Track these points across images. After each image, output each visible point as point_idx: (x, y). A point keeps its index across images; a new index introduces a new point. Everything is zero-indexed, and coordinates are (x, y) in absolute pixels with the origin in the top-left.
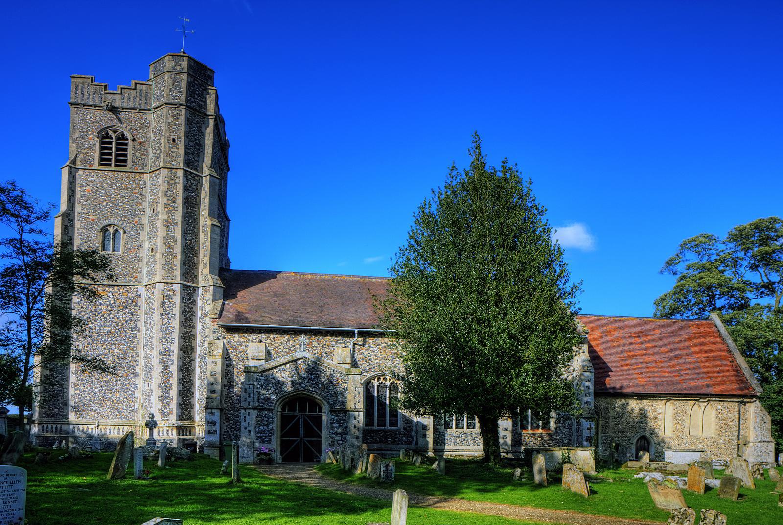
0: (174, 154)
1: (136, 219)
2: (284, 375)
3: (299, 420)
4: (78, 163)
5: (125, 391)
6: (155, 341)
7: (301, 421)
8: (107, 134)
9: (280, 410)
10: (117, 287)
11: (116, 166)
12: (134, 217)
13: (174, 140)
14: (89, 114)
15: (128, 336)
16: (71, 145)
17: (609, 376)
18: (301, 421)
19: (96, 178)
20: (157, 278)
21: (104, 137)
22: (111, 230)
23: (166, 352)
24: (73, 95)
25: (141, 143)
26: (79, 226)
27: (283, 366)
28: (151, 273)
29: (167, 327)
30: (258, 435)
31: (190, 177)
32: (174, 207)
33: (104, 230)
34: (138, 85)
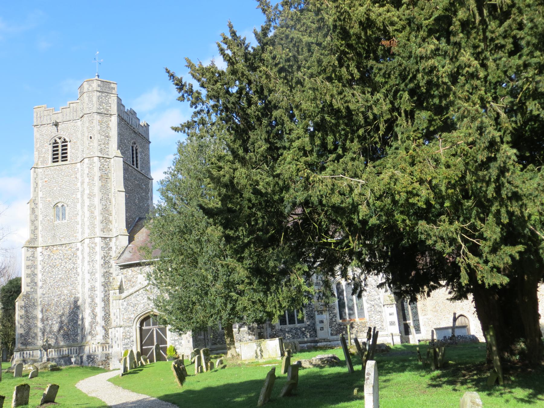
0: (91, 147)
1: (74, 196)
2: (138, 299)
3: (153, 330)
4: (40, 164)
6: (86, 282)
7: (155, 332)
8: (56, 141)
10: (64, 246)
11: (62, 161)
12: (73, 194)
13: (91, 138)
14: (44, 129)
15: (72, 279)
16: (35, 153)
18: (155, 332)
20: (86, 235)
22: (60, 205)
24: (35, 120)
26: (41, 207)
27: (137, 293)
28: (83, 233)
29: (93, 270)
30: (124, 346)
31: (103, 160)
32: (93, 184)
33: (56, 206)
34: (71, 105)
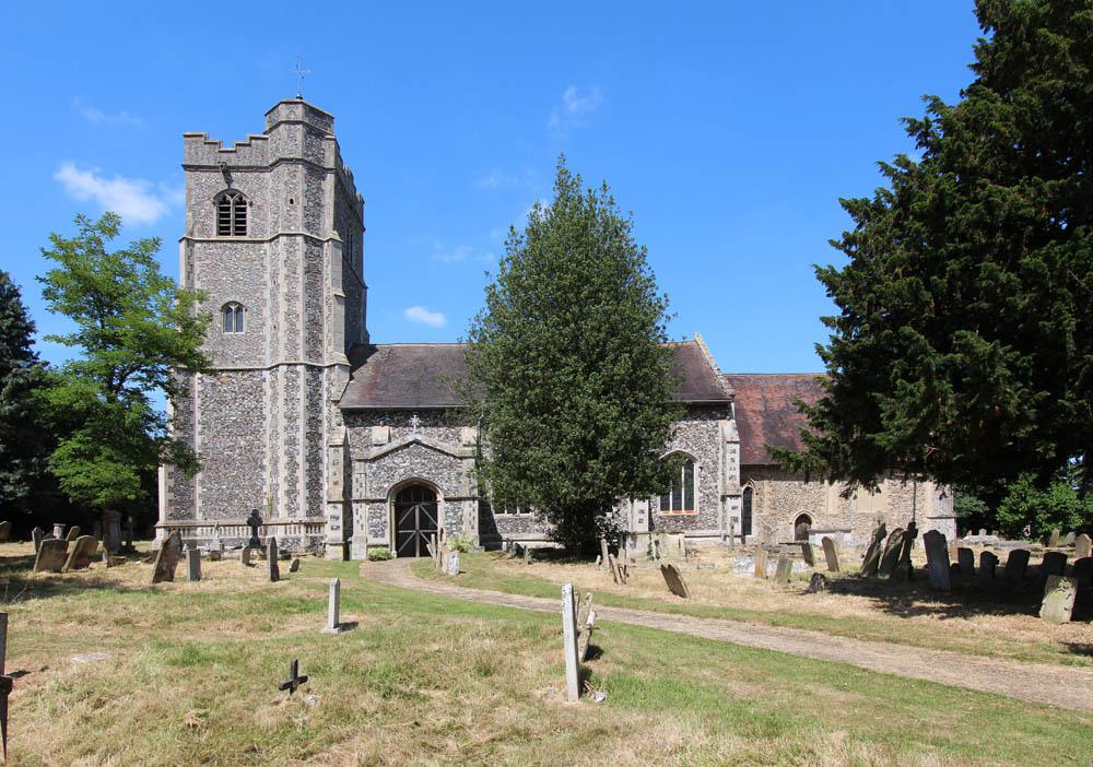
8: (225, 198)
12: (256, 291)
13: (292, 201)
23: (292, 442)
25: (259, 207)
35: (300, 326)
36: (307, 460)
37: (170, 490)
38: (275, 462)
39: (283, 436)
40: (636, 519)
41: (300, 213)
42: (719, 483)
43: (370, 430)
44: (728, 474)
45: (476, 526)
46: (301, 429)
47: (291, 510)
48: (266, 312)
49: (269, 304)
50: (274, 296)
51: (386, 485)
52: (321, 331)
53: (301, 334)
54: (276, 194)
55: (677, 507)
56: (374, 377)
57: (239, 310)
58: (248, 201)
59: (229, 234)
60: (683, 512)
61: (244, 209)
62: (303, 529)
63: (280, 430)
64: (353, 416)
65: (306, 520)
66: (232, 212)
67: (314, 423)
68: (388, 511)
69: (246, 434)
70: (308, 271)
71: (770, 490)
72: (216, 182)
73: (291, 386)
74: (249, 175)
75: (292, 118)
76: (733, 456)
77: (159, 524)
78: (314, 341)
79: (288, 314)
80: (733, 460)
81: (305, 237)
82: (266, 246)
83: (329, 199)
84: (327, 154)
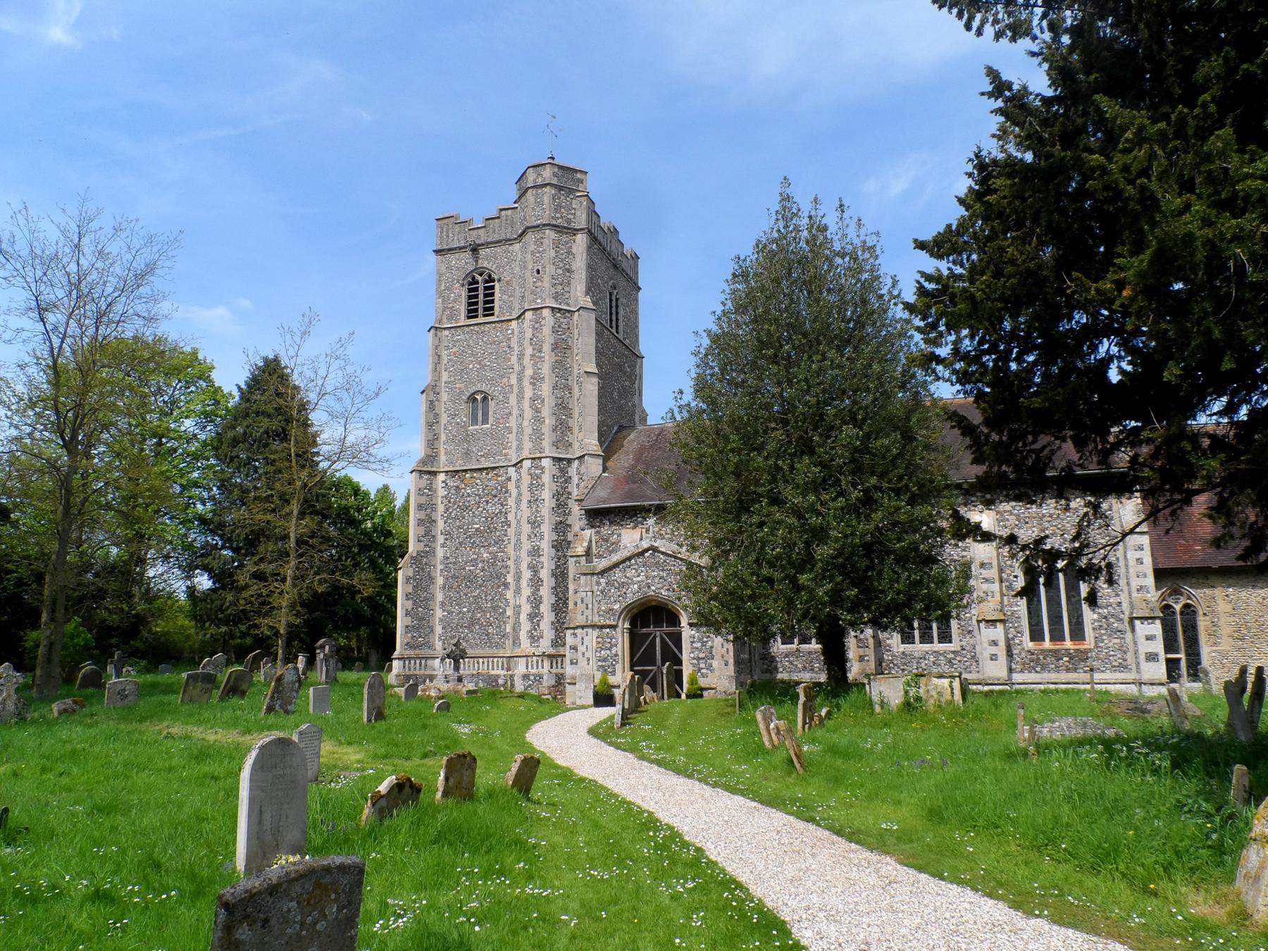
3: (655, 637)
5: (495, 608)
7: (658, 640)
8: (474, 278)
9: (627, 625)
12: (502, 377)
13: (538, 272)
17: (977, 477)
18: (658, 640)
19: (462, 337)
21: (470, 284)
23: (535, 552)
25: (508, 282)
33: (472, 398)
35: (546, 412)
36: (554, 575)
37: (407, 613)
38: (518, 577)
39: (526, 546)
40: (986, 654)
41: (547, 283)
42: (1124, 598)
43: (619, 535)
44: (1135, 583)
45: (731, 661)
46: (546, 537)
47: (534, 639)
48: (513, 399)
49: (516, 390)
50: (520, 380)
51: (617, 607)
52: (570, 416)
53: (547, 421)
54: (524, 267)
55: (1057, 636)
56: (634, 467)
57: (485, 399)
58: (496, 277)
59: (476, 317)
60: (1047, 644)
61: (493, 288)
62: (547, 663)
63: (524, 538)
64: (596, 516)
65: (551, 651)
66: (481, 293)
67: (561, 527)
68: (621, 641)
69: (489, 545)
70: (555, 347)
71: (1229, 608)
72: (464, 262)
73: (536, 484)
74: (498, 250)
75: (540, 181)
76: (1138, 554)
77: (396, 654)
78: (563, 428)
79: (533, 400)
80: (1140, 561)
81: (553, 308)
82: (514, 323)
83: (580, 263)
84: (578, 213)
